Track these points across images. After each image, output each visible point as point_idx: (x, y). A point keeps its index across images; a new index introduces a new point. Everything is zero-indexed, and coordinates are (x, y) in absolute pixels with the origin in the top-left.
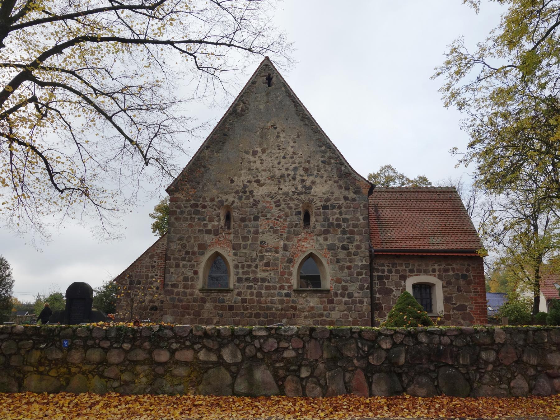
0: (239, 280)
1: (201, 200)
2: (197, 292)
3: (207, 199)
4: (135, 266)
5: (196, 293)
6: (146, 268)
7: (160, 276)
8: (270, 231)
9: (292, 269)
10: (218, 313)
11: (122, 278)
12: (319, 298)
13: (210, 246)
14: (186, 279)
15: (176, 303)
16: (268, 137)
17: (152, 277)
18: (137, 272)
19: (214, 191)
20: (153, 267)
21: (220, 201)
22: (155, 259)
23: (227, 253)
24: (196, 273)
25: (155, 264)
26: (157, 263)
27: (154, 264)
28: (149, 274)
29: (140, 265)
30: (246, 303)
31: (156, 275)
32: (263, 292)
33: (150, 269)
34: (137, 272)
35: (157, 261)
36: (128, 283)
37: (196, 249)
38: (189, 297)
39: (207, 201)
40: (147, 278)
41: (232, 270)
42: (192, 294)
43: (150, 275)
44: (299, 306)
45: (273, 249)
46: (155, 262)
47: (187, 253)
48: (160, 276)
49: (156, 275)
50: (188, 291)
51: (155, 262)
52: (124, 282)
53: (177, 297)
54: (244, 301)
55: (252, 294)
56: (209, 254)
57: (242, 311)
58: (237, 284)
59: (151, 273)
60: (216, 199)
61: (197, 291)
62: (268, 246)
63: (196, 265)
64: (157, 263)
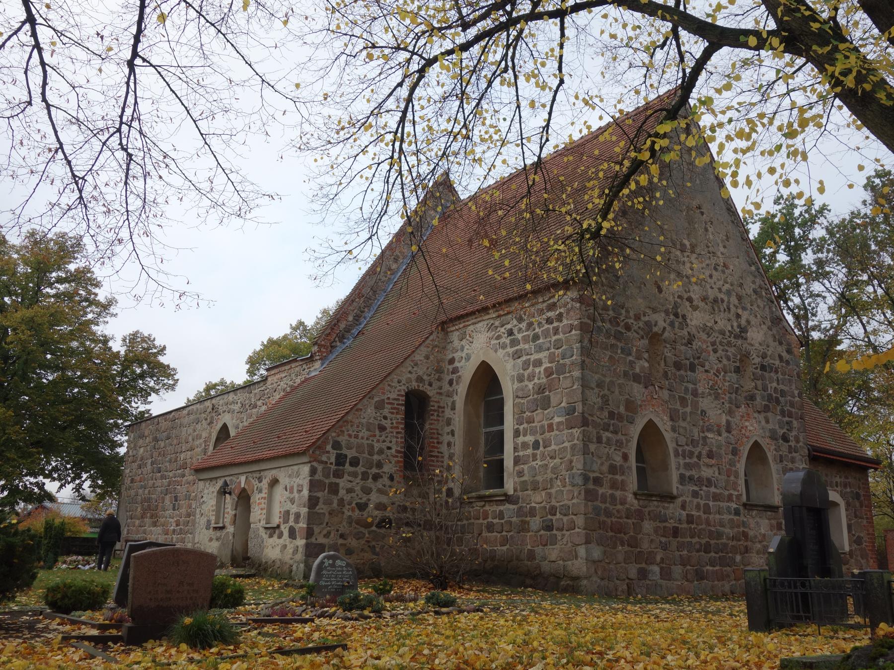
0: (682, 478)
1: (623, 311)
2: (630, 497)
3: (632, 314)
4: (347, 421)
5: (629, 499)
6: (368, 430)
7: (397, 451)
8: (710, 395)
9: (738, 465)
10: (661, 542)
11: (319, 447)
12: (769, 519)
13: (641, 406)
14: (613, 469)
15: (603, 518)
16: (696, 226)
17: (381, 452)
18: (350, 436)
19: (640, 301)
20: (382, 428)
21: (646, 323)
22: (386, 412)
23: (664, 424)
24: (625, 457)
25: (387, 423)
26: (389, 421)
27: (384, 422)
28: (376, 445)
29: (357, 421)
30: (693, 523)
31: (389, 448)
32: (711, 503)
33: (377, 432)
34: (350, 436)
35: (389, 415)
36: (333, 460)
37: (622, 409)
38: (619, 507)
39: (630, 318)
40: (371, 454)
41: (673, 461)
42: (623, 502)
43: (377, 446)
44: (751, 533)
45: (715, 429)
46: (385, 418)
47: (612, 415)
48: (397, 451)
49: (389, 448)
50: (618, 493)
51: (385, 418)
52: (324, 458)
53: (603, 506)
54: (690, 519)
55: (698, 507)
56: (640, 424)
57: (689, 539)
58: (680, 487)
59: (378, 441)
60: (643, 318)
61: (631, 495)
62: (708, 420)
63: (624, 441)
64: (389, 421)
